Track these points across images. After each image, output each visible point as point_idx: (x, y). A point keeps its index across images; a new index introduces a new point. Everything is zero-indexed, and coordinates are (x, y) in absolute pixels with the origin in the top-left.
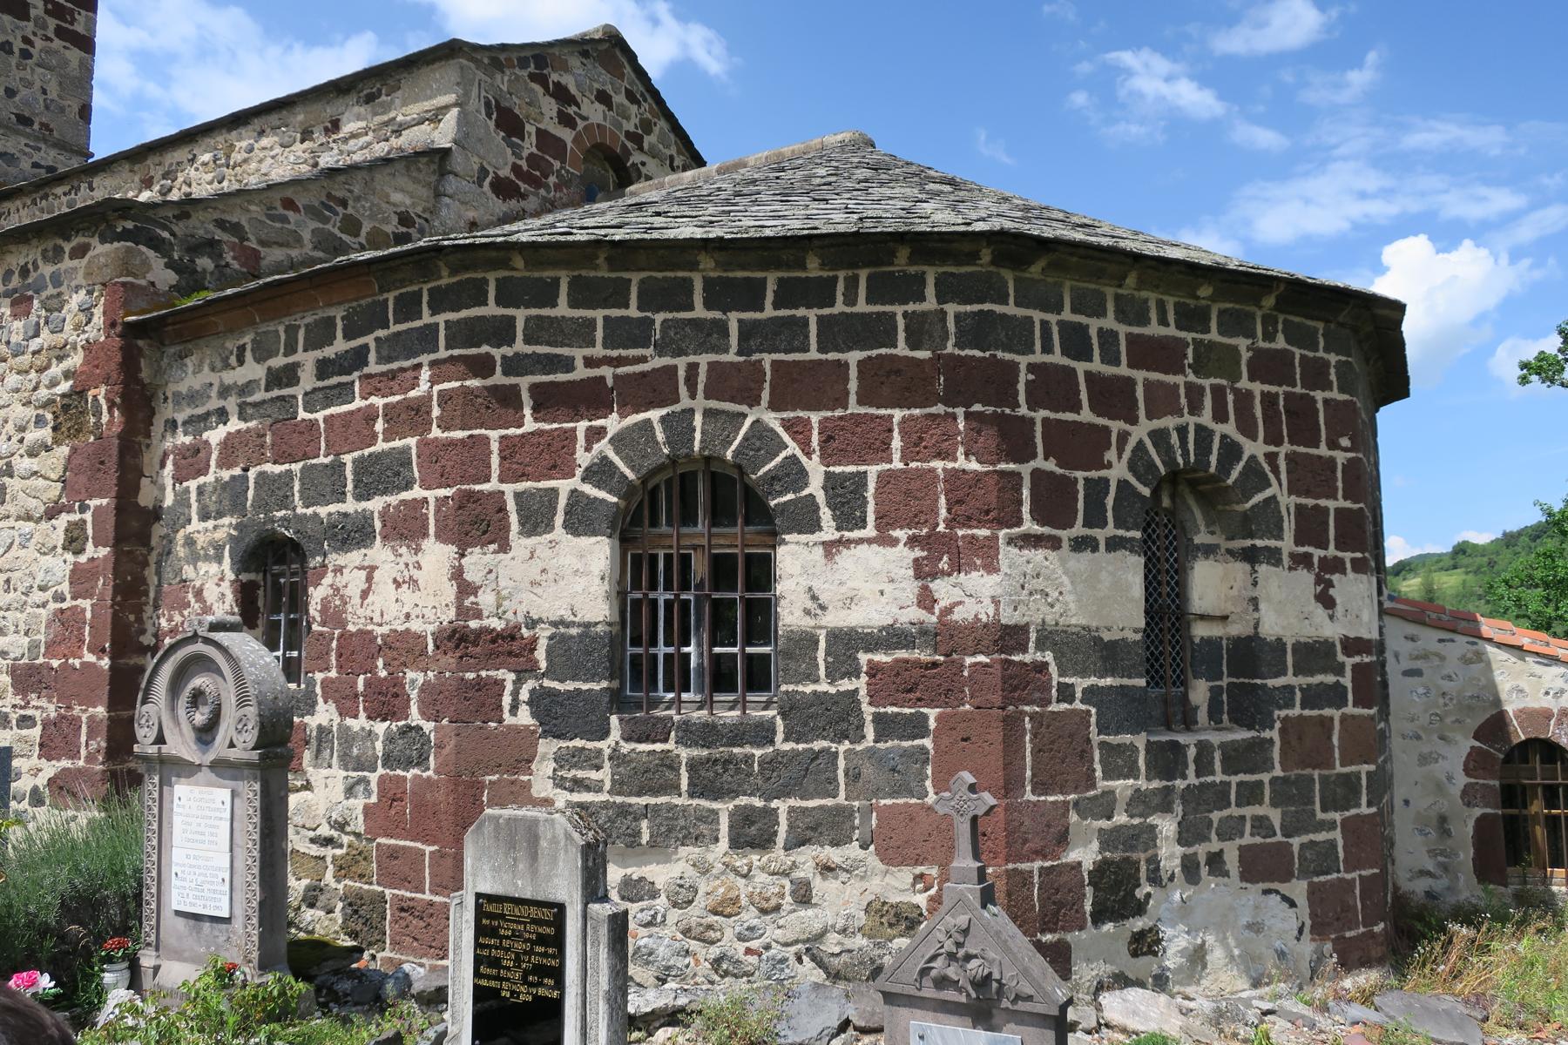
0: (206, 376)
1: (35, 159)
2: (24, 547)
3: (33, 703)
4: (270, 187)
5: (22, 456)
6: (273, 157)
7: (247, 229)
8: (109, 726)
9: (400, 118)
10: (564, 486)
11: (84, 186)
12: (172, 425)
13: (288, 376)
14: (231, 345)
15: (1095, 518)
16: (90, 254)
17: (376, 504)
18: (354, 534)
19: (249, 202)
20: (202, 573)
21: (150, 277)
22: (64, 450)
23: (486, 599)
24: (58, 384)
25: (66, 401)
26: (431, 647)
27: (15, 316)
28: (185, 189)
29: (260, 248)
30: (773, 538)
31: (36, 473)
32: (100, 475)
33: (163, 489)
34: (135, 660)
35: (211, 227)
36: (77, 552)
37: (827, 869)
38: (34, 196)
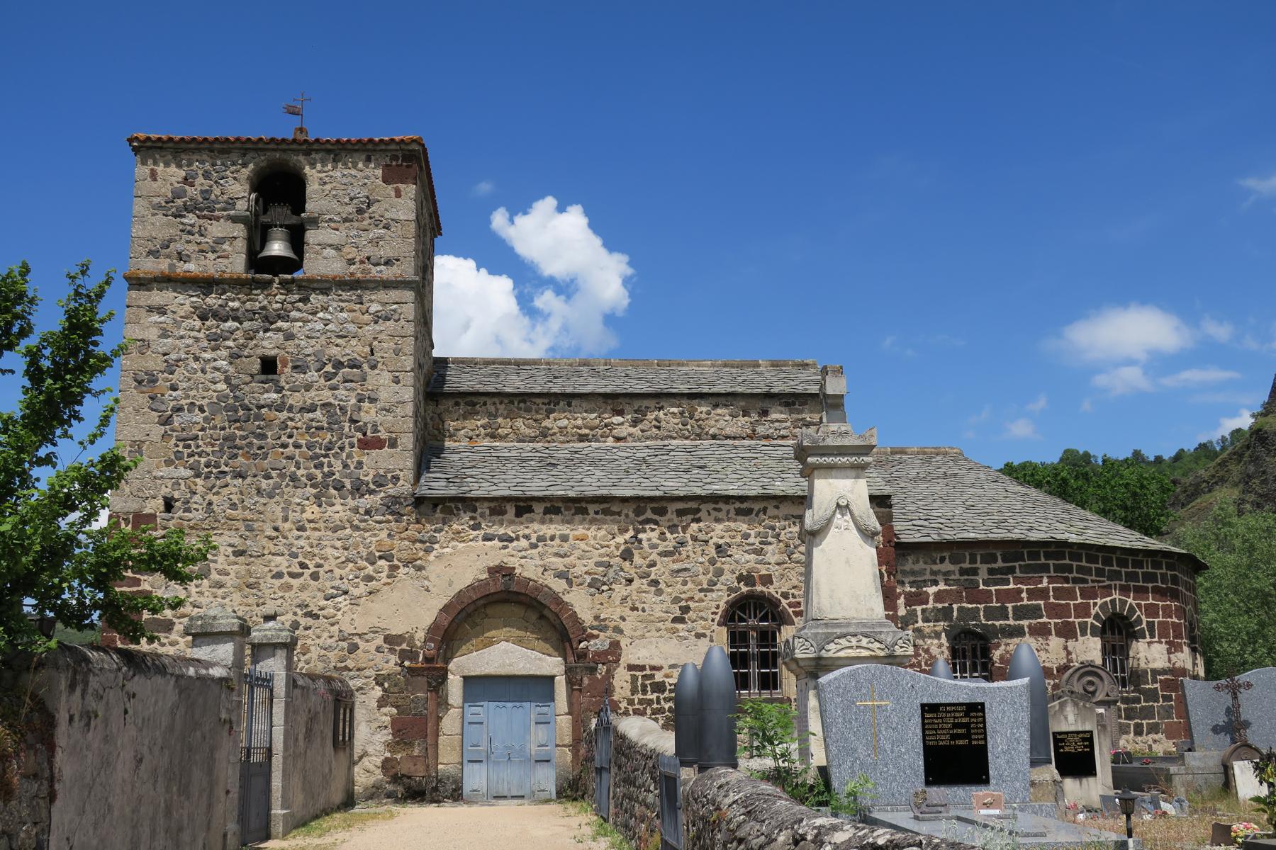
0: (921, 565)
9: (808, 419)
13: (974, 572)
17: (1025, 623)
23: (1074, 656)
26: (1055, 672)
37: (1155, 741)
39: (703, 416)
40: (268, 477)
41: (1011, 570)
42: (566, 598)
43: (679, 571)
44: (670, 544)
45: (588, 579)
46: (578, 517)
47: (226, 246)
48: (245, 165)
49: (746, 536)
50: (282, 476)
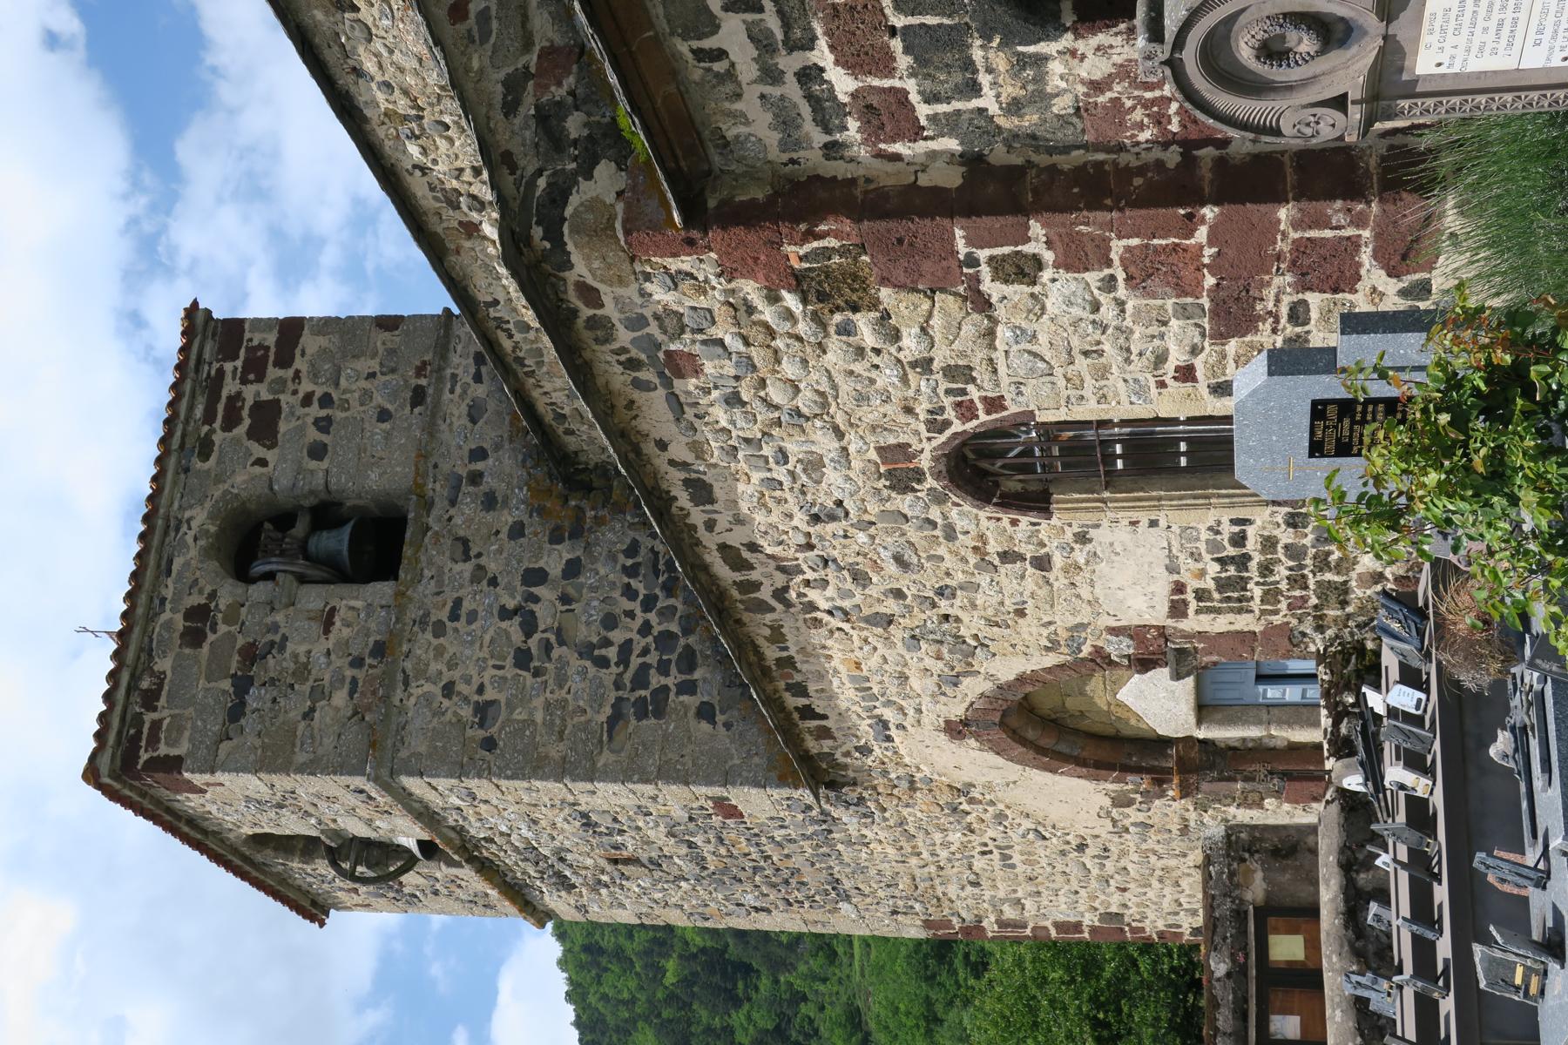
0: (749, 104)
1: (469, 379)
2: (1034, 336)
3: (1270, 306)
4: (438, 42)
5: (900, 349)
6: (391, 52)
7: (510, 70)
8: (1310, 199)
11: (493, 313)
12: (833, 150)
14: (696, 72)
16: (590, 281)
19: (467, 70)
20: (1063, 85)
21: (610, 198)
22: (885, 294)
24: (788, 310)
25: (812, 297)
27: (697, 371)
28: (468, 176)
29: (537, 48)
31: (923, 329)
32: (919, 243)
33: (933, 155)
34: (1206, 172)
35: (517, 121)
36: (1038, 263)
38: (521, 375)
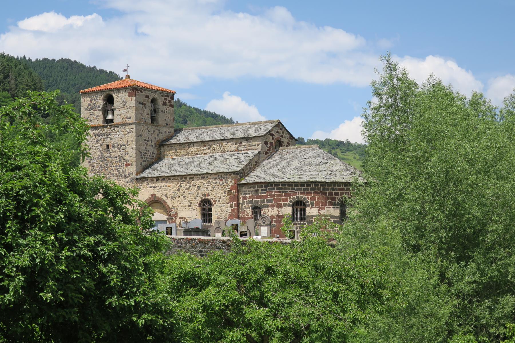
0: (246, 189)
10: (287, 203)
13: (258, 190)
15: (335, 205)
17: (269, 204)
18: (267, 206)
23: (281, 213)
30: (306, 207)
39: (225, 146)
40: (108, 175)
41: (266, 190)
42: (166, 201)
43: (190, 193)
44: (187, 187)
45: (171, 196)
46: (169, 181)
47: (99, 117)
48: (101, 96)
49: (204, 184)
50: (111, 174)
